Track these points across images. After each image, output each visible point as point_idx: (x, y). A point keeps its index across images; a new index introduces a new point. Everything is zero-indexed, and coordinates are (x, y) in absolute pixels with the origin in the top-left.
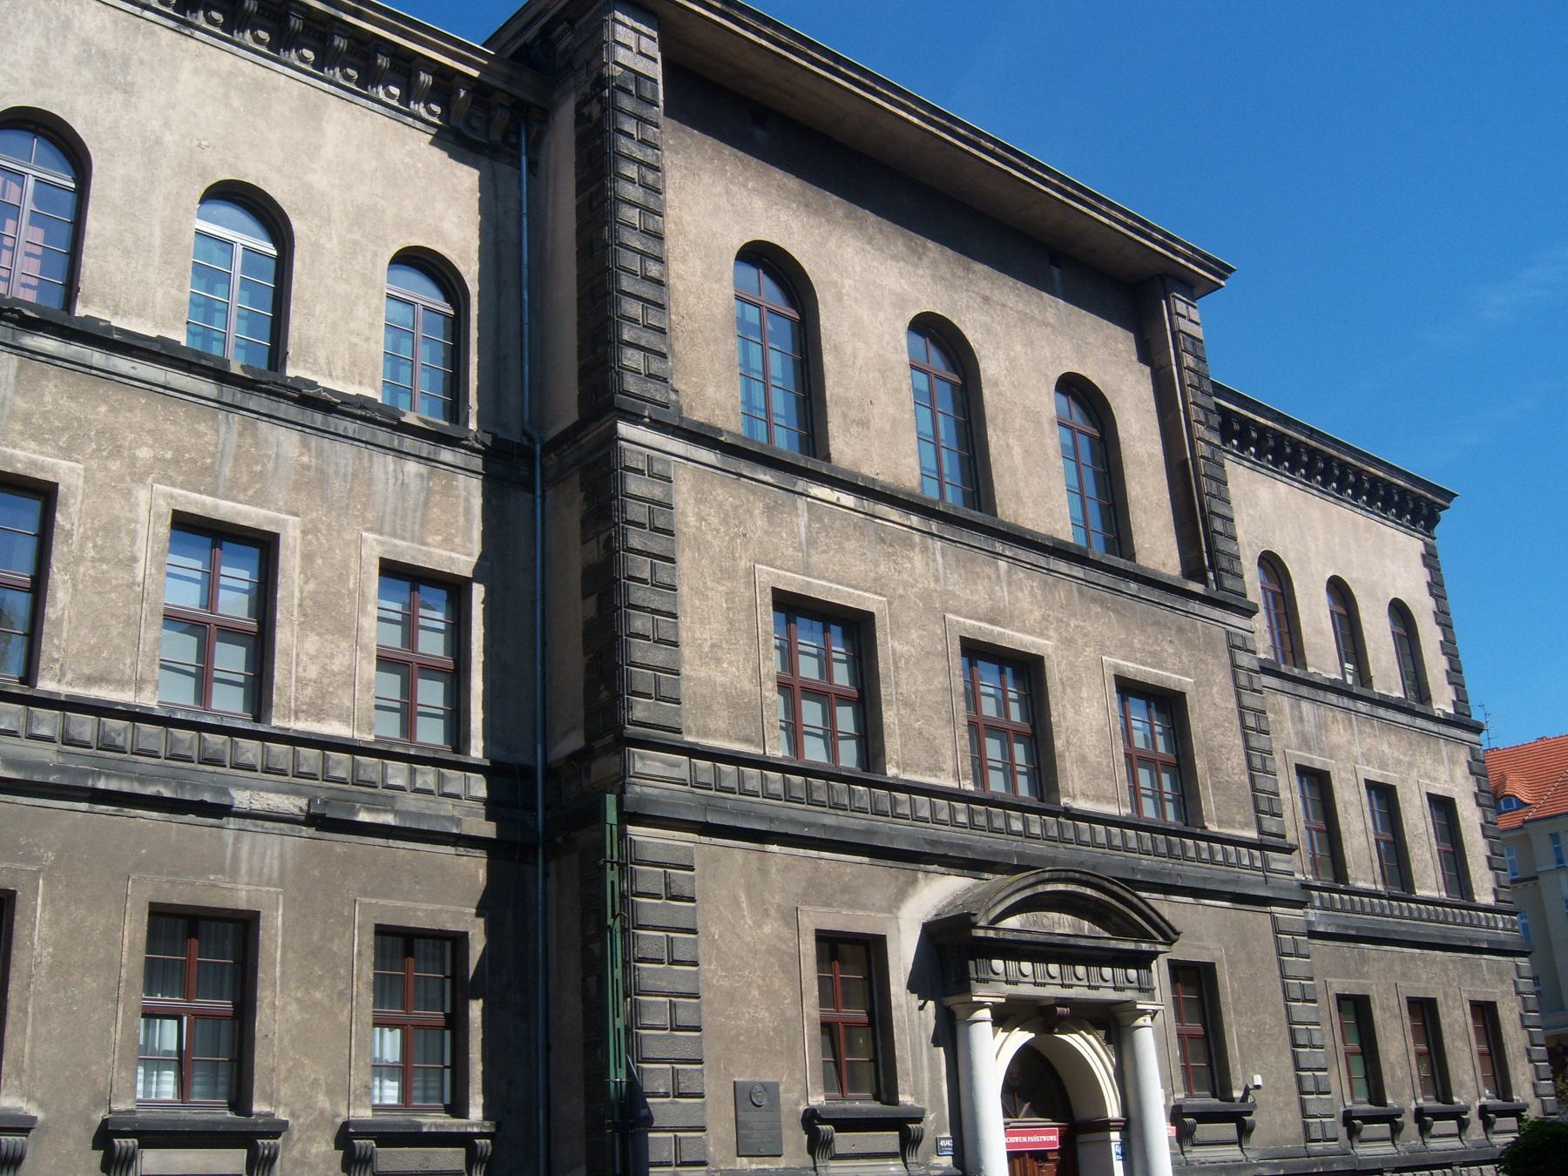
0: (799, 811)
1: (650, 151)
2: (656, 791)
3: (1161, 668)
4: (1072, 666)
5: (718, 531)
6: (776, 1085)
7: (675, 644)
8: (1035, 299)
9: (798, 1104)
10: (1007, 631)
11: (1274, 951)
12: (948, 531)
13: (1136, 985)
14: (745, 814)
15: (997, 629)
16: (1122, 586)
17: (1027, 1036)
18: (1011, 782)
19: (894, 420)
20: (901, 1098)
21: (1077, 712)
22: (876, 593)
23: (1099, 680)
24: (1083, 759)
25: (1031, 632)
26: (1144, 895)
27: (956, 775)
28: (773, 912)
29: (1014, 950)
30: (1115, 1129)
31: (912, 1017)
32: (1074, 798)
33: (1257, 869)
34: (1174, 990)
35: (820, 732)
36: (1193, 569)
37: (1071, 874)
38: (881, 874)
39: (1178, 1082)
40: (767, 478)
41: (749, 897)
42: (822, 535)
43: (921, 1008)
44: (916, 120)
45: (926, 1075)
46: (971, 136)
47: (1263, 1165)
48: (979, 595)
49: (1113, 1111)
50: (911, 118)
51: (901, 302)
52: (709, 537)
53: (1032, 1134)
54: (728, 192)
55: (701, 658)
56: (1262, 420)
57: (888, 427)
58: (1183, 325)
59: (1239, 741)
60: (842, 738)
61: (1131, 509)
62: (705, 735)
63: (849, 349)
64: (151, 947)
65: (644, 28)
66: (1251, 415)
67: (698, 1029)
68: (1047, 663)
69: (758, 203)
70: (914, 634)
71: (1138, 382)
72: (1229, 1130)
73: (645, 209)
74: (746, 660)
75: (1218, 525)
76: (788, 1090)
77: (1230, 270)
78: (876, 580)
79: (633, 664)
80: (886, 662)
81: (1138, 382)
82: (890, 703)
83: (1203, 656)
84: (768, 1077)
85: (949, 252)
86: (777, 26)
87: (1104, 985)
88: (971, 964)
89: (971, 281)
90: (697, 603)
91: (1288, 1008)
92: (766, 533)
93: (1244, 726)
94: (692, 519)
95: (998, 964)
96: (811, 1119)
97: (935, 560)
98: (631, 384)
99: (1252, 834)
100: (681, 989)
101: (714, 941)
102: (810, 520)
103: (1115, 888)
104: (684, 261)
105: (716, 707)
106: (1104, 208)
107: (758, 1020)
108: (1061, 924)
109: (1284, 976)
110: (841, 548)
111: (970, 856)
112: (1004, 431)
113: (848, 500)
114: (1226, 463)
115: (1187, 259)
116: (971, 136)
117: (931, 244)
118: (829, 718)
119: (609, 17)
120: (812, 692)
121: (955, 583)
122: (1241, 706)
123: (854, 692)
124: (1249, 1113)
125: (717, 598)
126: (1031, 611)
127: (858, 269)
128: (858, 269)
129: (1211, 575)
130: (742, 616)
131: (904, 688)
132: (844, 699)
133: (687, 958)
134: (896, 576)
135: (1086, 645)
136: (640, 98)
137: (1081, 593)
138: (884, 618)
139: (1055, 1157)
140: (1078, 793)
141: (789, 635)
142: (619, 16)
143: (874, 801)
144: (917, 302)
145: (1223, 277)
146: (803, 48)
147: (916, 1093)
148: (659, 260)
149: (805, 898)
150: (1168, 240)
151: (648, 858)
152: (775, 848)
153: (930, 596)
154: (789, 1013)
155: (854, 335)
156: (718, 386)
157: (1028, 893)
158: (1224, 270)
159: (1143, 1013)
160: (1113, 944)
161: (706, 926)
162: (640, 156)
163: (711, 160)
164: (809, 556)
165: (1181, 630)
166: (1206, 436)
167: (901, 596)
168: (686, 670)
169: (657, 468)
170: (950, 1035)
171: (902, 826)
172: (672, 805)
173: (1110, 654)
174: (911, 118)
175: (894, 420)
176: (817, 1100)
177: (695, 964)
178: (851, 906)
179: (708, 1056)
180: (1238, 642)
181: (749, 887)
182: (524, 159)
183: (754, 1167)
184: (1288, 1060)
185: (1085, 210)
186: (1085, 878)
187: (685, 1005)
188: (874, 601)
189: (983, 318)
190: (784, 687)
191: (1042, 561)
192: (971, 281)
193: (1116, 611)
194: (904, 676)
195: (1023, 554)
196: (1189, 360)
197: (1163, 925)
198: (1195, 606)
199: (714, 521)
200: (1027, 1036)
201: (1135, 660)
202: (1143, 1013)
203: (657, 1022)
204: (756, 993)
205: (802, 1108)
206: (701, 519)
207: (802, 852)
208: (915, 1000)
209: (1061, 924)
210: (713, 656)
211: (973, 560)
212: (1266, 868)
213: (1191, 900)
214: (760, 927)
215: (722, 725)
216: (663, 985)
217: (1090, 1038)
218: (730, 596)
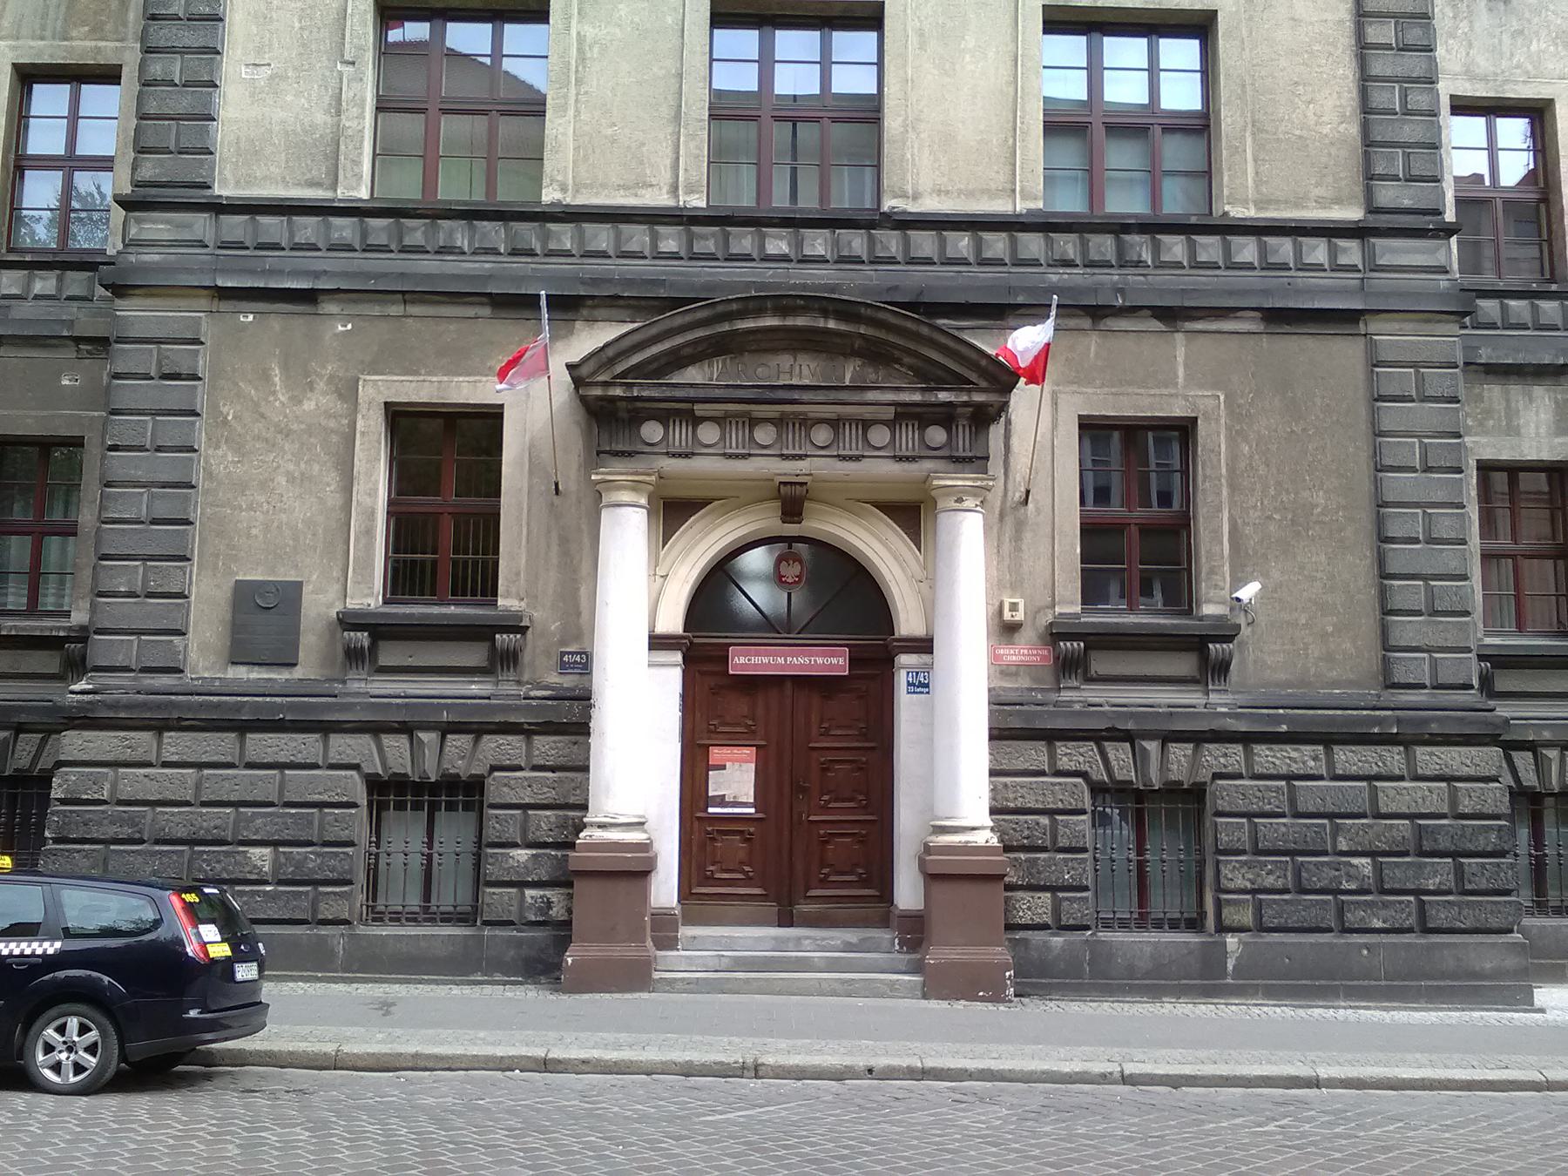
9: (331, 605)
14: (368, 276)
26: (941, 322)
32: (916, 197)
34: (587, 434)
41: (285, 368)
47: (1237, 716)
84: (287, 575)
95: (652, 431)
99: (1353, 213)
101: (225, 422)
105: (268, 150)
111: (663, 293)
147: (531, 596)
161: (214, 407)
183: (254, 675)
204: (282, 480)
214: (300, 402)
216: (141, 474)
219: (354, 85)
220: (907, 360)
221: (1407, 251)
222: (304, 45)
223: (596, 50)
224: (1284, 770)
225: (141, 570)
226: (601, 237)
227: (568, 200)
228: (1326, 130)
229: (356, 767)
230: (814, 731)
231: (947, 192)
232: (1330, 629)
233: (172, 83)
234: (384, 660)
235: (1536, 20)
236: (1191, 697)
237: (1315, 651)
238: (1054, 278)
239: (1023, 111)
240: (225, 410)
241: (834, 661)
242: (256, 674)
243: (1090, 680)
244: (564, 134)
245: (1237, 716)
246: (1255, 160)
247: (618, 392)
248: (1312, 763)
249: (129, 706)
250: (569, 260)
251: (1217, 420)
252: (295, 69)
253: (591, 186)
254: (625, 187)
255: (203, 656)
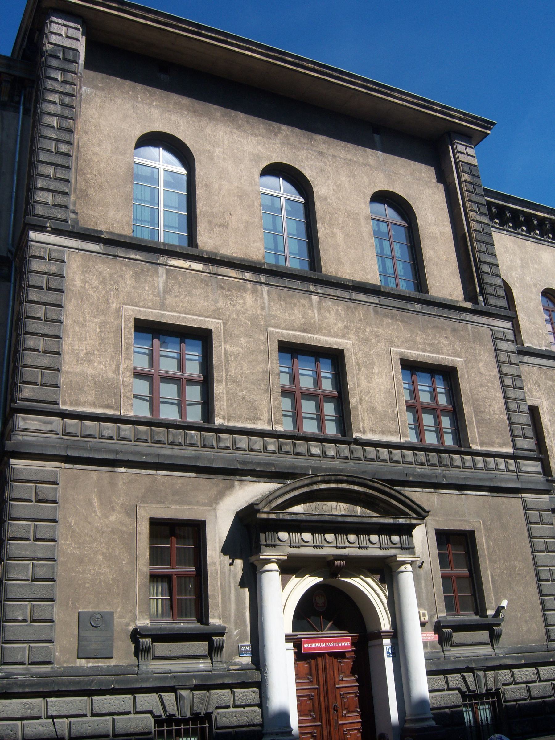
0: (141, 447)
1: (68, 86)
2: (34, 439)
3: (438, 353)
4: (367, 355)
5: (97, 288)
6: (112, 614)
7: (58, 353)
8: (360, 152)
9: (128, 625)
10: (315, 336)
11: (524, 521)
12: (273, 281)
13: (399, 545)
14: (97, 450)
15: (307, 335)
16: (409, 307)
17: (316, 580)
18: (440, 437)
19: (247, 222)
20: (211, 621)
21: (370, 381)
22: (215, 318)
23: (387, 362)
24: (372, 410)
25: (337, 336)
27: (270, 422)
28: (118, 508)
29: (297, 526)
30: (387, 637)
31: (223, 571)
32: (364, 432)
33: (513, 471)
35: (434, 429)
36: (470, 295)
37: (339, 477)
38: (208, 484)
39: (441, 605)
40: (138, 257)
41: (100, 499)
42: (176, 288)
43: (231, 564)
44: (257, 56)
45: (233, 606)
46: (297, 61)
47: (508, 658)
48: (296, 315)
49: (386, 625)
50: (254, 55)
51: (257, 158)
52: (91, 292)
53: (330, 642)
54: (134, 107)
55: (77, 361)
56: (540, 214)
57: (242, 227)
58: (461, 157)
59: (500, 395)
60: (189, 405)
61: (426, 263)
62: (78, 404)
63: (216, 186)
64: (151, 543)
65: (71, 24)
66: (532, 211)
67: (53, 580)
68: (346, 354)
69: (156, 112)
70: (243, 341)
71: (434, 193)
72: (484, 635)
73: (62, 117)
74: (112, 360)
75: (485, 268)
76: (120, 617)
77: (493, 124)
78: (215, 311)
79: (25, 366)
80: (219, 358)
81: (434, 193)
82: (220, 381)
83: (473, 346)
84: (105, 608)
85: (297, 130)
86: (156, 13)
87: (374, 546)
88: (262, 536)
89: (312, 145)
90: (78, 329)
91: (534, 557)
92: (134, 287)
93: (503, 385)
94: (78, 282)
95: (284, 535)
96: (136, 635)
97: (262, 297)
98: (40, 210)
99: (509, 450)
100: (40, 555)
101: (70, 526)
102: (167, 278)
103: (376, 485)
104: (99, 145)
105: (86, 388)
106: (396, 95)
107: (101, 574)
108: (339, 509)
109: (531, 537)
110: (190, 293)
111: (274, 469)
112: (330, 225)
113: (198, 266)
114: (493, 233)
115: (461, 119)
116: (297, 61)
117: (284, 127)
118: (438, 422)
119: (48, 21)
120: (427, 409)
121: (278, 310)
122: (501, 373)
123: (450, 407)
124: (499, 625)
125: (93, 325)
126: (335, 324)
127: (226, 142)
128: (226, 142)
129: (481, 298)
130: (112, 335)
131: (232, 372)
132: (328, 398)
133: (47, 537)
134: (231, 308)
135: (378, 342)
136: (65, 59)
137: (376, 312)
138: (219, 332)
139: (353, 655)
140: (365, 428)
141: (413, 381)
142: (54, 19)
143: (203, 440)
144: (269, 157)
145: (489, 129)
146: (175, 23)
147: (225, 617)
148: (69, 143)
149: (144, 499)
150: (445, 110)
151: (22, 478)
152: (123, 470)
153: (256, 318)
154: (125, 569)
155: (221, 178)
156: (117, 211)
157: (305, 490)
158: (489, 125)
159: (404, 563)
160: (382, 521)
161: (65, 517)
162: (60, 89)
163: (128, 92)
164: (164, 298)
165: (454, 330)
166: (477, 220)
167: (234, 319)
168: (65, 368)
169: (54, 255)
170: (251, 580)
171: (224, 453)
172: (42, 446)
173: (398, 347)
174: (254, 55)
175: (247, 222)
176: (143, 622)
177: (54, 540)
178: (179, 504)
179: (58, 596)
180: (500, 335)
181: (100, 494)
182: (22, 108)
183: (90, 665)
184: (534, 589)
185: (383, 97)
186: (351, 479)
187: (43, 566)
188: (212, 322)
189: (318, 164)
190: (410, 407)
191: (346, 295)
192: (312, 145)
193: (405, 322)
194: (233, 365)
195: (331, 291)
196: (466, 177)
197: (415, 507)
198: (468, 316)
199: (95, 283)
200: (316, 580)
201: (418, 349)
202: (404, 563)
203: (20, 576)
204: (100, 557)
205: (131, 628)
206: (85, 281)
207: (143, 471)
208: (227, 560)
209: (339, 509)
210: (88, 358)
211: (291, 297)
212: (518, 469)
213: (456, 492)
214: (107, 517)
215: (89, 398)
216: (28, 554)
217: (369, 580)
218: (103, 325)
219: (127, 361)
220: (381, 504)
221: (530, 465)
222: (102, 340)
223: (233, 357)
224: (525, 680)
225: (29, 607)
226: (242, 441)
227: (226, 424)
228: (497, 417)
229: (150, 712)
230: (337, 679)
231: (375, 431)
232: (528, 618)
233: (38, 351)
234: (158, 653)
235: (528, 376)
236: (203, 665)
237: (525, 628)
238: (419, 470)
239: (399, 400)
240: (70, 520)
241: (346, 644)
242: (91, 664)
243: (453, 646)
244: (222, 393)
245: (508, 658)
246: (477, 427)
247: (273, 516)
248: (533, 676)
249: (30, 685)
250: (259, 454)
251: (481, 532)
252: (98, 350)
253: (235, 418)
254: (250, 419)
255: (65, 655)
